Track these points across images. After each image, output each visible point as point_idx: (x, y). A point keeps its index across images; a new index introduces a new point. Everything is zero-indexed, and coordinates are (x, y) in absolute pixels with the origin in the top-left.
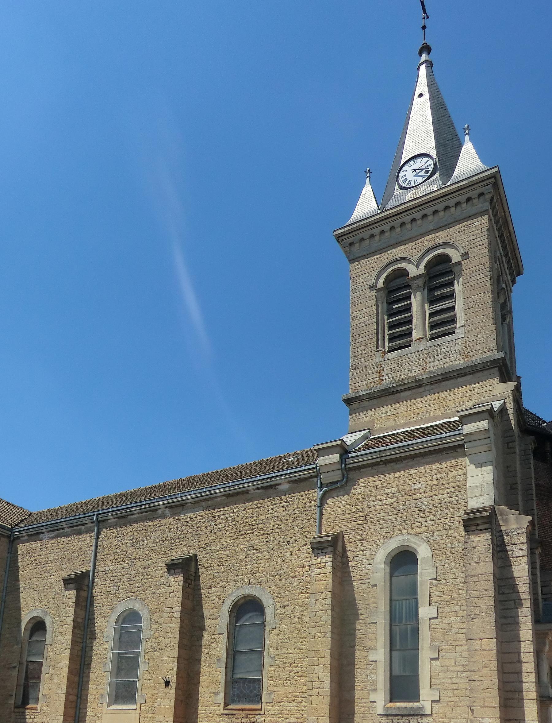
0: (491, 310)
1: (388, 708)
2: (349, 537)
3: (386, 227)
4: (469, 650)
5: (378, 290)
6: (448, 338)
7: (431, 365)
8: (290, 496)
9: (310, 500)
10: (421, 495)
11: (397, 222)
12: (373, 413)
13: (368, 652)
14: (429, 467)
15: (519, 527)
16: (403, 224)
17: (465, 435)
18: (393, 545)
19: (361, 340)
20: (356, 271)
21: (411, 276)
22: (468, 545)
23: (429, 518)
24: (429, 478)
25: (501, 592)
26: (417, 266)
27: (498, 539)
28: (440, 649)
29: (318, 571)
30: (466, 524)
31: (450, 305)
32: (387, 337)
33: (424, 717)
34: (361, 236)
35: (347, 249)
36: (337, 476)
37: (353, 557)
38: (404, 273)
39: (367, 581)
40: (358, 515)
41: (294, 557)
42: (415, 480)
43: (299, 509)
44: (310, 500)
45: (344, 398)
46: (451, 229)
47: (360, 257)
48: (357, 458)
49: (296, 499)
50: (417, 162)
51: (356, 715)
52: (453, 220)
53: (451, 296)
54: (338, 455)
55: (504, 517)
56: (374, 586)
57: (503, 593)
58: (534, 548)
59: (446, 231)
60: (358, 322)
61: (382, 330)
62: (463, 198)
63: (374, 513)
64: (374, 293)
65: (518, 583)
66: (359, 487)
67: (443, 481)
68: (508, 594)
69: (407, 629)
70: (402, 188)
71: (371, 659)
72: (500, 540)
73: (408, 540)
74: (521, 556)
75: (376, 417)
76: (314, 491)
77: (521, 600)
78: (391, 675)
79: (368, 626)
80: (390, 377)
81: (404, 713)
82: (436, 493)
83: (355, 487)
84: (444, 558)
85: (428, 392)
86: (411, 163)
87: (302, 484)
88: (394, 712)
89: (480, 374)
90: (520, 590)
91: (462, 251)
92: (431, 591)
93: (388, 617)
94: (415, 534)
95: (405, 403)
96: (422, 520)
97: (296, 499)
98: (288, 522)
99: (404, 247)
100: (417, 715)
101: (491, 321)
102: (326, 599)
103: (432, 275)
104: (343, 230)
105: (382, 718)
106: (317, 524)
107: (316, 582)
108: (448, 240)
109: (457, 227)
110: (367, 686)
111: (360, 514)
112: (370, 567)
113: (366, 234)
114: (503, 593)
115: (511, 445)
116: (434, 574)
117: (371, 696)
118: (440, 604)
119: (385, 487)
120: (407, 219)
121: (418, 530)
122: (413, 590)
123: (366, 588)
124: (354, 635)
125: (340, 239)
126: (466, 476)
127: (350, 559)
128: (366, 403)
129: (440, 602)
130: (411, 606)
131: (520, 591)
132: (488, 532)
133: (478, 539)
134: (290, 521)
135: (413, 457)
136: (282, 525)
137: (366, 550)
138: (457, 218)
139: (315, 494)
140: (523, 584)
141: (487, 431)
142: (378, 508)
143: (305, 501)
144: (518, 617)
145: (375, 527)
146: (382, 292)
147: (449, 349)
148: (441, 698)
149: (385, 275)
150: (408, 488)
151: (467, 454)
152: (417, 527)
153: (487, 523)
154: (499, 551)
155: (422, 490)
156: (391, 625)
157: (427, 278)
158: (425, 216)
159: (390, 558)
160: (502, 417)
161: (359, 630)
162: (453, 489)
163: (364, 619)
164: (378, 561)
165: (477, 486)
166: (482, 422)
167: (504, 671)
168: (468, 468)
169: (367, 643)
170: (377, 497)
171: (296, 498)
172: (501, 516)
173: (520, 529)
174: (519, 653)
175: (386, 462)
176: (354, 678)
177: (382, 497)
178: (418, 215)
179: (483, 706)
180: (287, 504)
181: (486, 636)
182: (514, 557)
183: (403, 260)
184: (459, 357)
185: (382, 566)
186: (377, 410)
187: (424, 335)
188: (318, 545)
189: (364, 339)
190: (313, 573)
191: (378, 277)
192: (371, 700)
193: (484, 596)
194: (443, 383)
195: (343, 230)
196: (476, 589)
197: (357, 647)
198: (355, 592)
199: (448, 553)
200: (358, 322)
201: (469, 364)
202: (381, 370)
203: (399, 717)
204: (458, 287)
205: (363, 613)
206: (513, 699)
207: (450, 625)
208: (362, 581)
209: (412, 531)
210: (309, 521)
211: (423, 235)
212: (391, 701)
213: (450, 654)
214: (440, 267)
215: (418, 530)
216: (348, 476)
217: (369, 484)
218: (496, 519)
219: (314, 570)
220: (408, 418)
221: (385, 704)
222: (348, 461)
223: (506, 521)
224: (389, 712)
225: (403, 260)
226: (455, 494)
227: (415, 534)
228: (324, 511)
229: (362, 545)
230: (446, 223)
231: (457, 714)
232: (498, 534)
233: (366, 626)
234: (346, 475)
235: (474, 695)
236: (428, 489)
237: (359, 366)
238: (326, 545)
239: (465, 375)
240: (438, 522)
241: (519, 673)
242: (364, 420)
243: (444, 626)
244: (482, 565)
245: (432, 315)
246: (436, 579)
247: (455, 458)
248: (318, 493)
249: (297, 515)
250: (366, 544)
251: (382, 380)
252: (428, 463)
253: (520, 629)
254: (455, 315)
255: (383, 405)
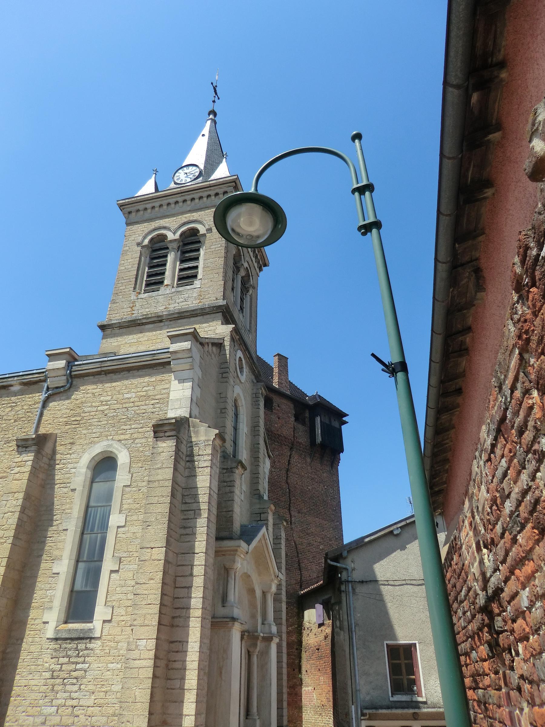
0: (222, 270)
1: (58, 630)
2: (61, 439)
3: (157, 204)
4: (140, 560)
5: (143, 247)
6: (188, 287)
7: (172, 306)
8: (19, 397)
9: (35, 402)
10: (130, 404)
11: (165, 202)
12: (120, 340)
13: (53, 563)
14: (141, 380)
15: (206, 438)
16: (169, 204)
17: (171, 353)
18: (98, 449)
19: (123, 281)
20: (130, 232)
21: (168, 239)
22: (155, 451)
23: (133, 426)
24: (139, 390)
25: (184, 501)
26: (174, 233)
27: (188, 449)
28: (122, 561)
29: (17, 470)
30: (156, 429)
31: (195, 265)
32: (144, 283)
33: (93, 641)
34: (137, 208)
35: (126, 215)
36: (61, 381)
37: (61, 460)
38: (163, 237)
39: (68, 485)
40: (73, 419)
41: (8, 456)
42: (128, 390)
43: (24, 410)
44: (35, 402)
45: (99, 324)
46: (203, 212)
47: (134, 223)
48: (81, 366)
49: (24, 401)
50: (189, 169)
51: (25, 640)
52: (205, 206)
53: (197, 259)
54: (65, 361)
55: (196, 429)
56: (73, 490)
57: (186, 503)
58: (233, 468)
59: (199, 213)
60: (123, 268)
61: (141, 277)
62: (212, 193)
63: (88, 418)
64: (139, 248)
65: (199, 493)
66: (80, 393)
67: (150, 393)
68: (190, 503)
69: (97, 537)
70: (176, 183)
71: (55, 571)
72: (189, 451)
73: (111, 446)
74: (205, 467)
75: (123, 343)
76: (41, 394)
77: (200, 510)
78: (72, 591)
79: (58, 532)
80: (139, 312)
81: (74, 636)
82: (143, 403)
83: (76, 393)
84: (140, 465)
85: (167, 327)
86: (185, 169)
87: (32, 387)
88: (64, 635)
89: (208, 316)
90: (201, 500)
91: (207, 227)
92: (124, 498)
93: (80, 524)
94: (118, 441)
95: (147, 334)
96: (128, 427)
97: (24, 401)
98: (10, 421)
99: (167, 220)
100: (87, 638)
101: (221, 278)
102: (17, 499)
103: (186, 242)
104: (124, 201)
105: (50, 643)
106: (35, 425)
107: (13, 481)
108: (199, 219)
109: (206, 211)
110: (43, 603)
111: (76, 418)
112: (73, 470)
113: (141, 207)
114: (186, 503)
115: (224, 375)
116: (128, 481)
117: (45, 615)
118: (129, 512)
119: (101, 395)
120: (172, 200)
121: (122, 437)
122: (109, 497)
123: (66, 492)
124: (44, 543)
125: (122, 208)
126: (170, 390)
127: (58, 462)
128: (117, 331)
129: (130, 510)
130: (105, 513)
131: (201, 501)
132: (173, 439)
133: (164, 445)
134: (12, 421)
135: (129, 370)
136: (5, 425)
137: (73, 453)
138: (208, 206)
139: (40, 397)
140: (204, 494)
141: (190, 350)
142: (92, 414)
143: (30, 403)
144: (196, 527)
145: (85, 432)
146: (146, 249)
147: (188, 295)
148: (114, 617)
149: (150, 237)
150: (121, 396)
151: (173, 370)
152: (122, 434)
153: (173, 430)
154: (188, 461)
155: (132, 400)
156: (82, 534)
157: (181, 244)
158: (185, 201)
159: (94, 463)
160: (220, 351)
161: (50, 537)
162: (158, 401)
163: (57, 525)
164: (82, 465)
165: (177, 399)
166: (186, 343)
167: (176, 586)
168: (172, 382)
169: (54, 553)
170: (93, 404)
171: (23, 399)
172: (193, 427)
173: (208, 441)
174: (192, 566)
175: (107, 373)
176: (34, 593)
177: (97, 404)
178: (180, 199)
179: (142, 624)
180: (14, 404)
181: (157, 545)
182: (200, 468)
183: (165, 228)
184: (194, 302)
185: (84, 470)
186: (124, 337)
187: (172, 283)
188: (23, 443)
189: (126, 281)
190: (12, 472)
191: (145, 238)
192: (44, 620)
193: (161, 502)
194: (179, 321)
195: (124, 201)
196: (155, 495)
197: (44, 557)
198: (55, 496)
199: (144, 461)
200: (123, 268)
201: (200, 307)
202: (133, 306)
203: (69, 641)
204: (202, 252)
205: (57, 519)
206: (179, 617)
207: (135, 534)
208: (64, 484)
209: (116, 437)
210: (30, 421)
211: (183, 213)
212: (66, 622)
213: (131, 567)
214: (193, 238)
215: (122, 437)
216: (72, 382)
217: (88, 391)
218: (188, 431)
219: (14, 468)
220: (148, 346)
221: (57, 625)
222: (74, 368)
223: (197, 433)
224: (59, 636)
225: (165, 228)
226: (157, 406)
227: (118, 441)
228: (45, 414)
229: (71, 448)
230: (199, 208)
231: (125, 636)
232: (189, 445)
233: (58, 533)
234: (70, 381)
235: (136, 612)
236: (136, 399)
237: (117, 301)
238: (30, 442)
239: (196, 315)
240: (140, 430)
241: (189, 587)
242: (113, 344)
243: (129, 535)
244: (163, 470)
245: (181, 270)
246: (129, 486)
247: (163, 373)
248: (41, 397)
249: (20, 416)
250: (75, 448)
251: (133, 314)
252: (140, 376)
253: (197, 540)
254: (198, 272)
255: (131, 333)
